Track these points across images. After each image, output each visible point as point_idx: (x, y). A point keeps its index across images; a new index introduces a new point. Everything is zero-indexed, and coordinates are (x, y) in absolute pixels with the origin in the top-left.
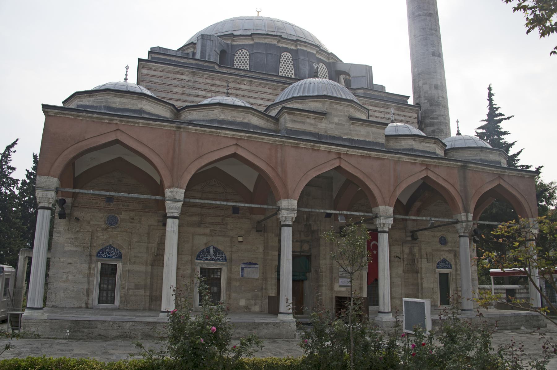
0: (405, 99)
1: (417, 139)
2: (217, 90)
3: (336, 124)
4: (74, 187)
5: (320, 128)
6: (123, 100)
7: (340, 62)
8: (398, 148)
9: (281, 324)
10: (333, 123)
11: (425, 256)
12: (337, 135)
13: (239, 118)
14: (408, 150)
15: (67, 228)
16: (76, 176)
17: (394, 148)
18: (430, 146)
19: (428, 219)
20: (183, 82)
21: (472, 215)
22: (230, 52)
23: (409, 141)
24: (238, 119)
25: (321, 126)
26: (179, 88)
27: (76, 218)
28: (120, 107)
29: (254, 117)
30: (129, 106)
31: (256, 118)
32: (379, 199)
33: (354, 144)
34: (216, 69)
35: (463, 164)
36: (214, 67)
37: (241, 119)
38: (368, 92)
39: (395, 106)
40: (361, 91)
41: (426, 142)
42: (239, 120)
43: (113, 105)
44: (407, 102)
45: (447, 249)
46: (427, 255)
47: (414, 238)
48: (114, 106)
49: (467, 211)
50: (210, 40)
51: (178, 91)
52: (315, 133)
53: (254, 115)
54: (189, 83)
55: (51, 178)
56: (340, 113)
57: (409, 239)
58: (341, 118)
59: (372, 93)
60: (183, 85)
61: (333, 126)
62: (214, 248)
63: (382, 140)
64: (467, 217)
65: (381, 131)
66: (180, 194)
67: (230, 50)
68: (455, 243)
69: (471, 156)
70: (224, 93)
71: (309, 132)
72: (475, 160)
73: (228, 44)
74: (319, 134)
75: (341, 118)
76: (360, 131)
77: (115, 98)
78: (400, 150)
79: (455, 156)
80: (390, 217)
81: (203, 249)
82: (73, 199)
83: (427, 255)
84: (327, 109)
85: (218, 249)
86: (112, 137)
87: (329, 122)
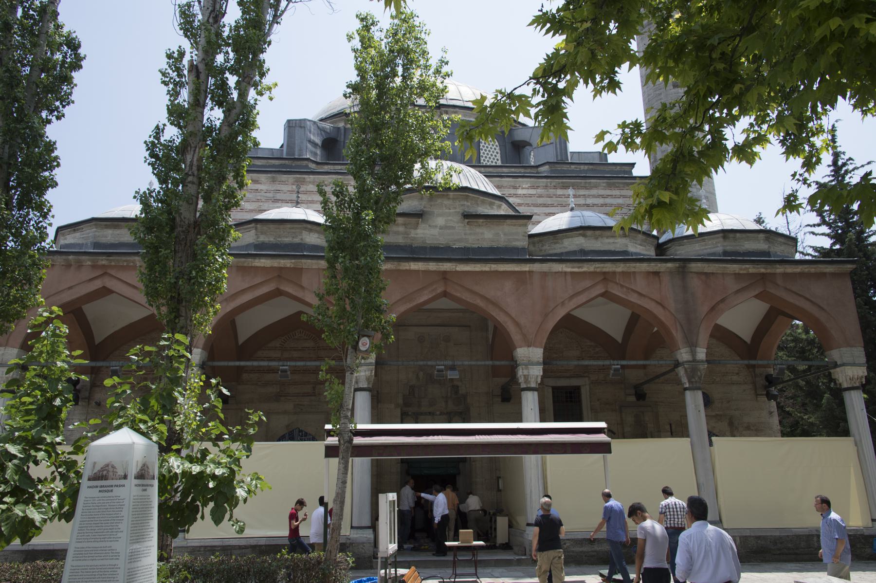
0: (627, 168)
1: (589, 233)
2: (310, 199)
3: (441, 228)
4: (239, 360)
5: (415, 238)
6: (117, 232)
7: (521, 127)
8: (558, 251)
9: (348, 545)
10: (436, 226)
11: (668, 427)
12: (442, 244)
13: (287, 237)
14: (574, 253)
15: (84, 418)
16: (240, 344)
17: (551, 252)
18: (616, 241)
19: (607, 362)
20: (258, 194)
21: (705, 350)
22: (342, 140)
23: (576, 239)
24: (286, 239)
25: (417, 234)
26: (253, 203)
27: (96, 403)
28: (113, 242)
29: (311, 234)
30: (126, 239)
31: (316, 235)
32: (516, 337)
33: (468, 255)
34: (311, 168)
35: (677, 265)
36: (307, 167)
37: (291, 239)
38: (559, 167)
39: (604, 183)
40: (546, 168)
41: (607, 237)
42: (287, 240)
43: (103, 240)
44: (632, 173)
45: (714, 414)
46: (671, 425)
47: (641, 396)
48: (104, 242)
49: (692, 346)
50: (301, 127)
51: (251, 208)
52: (406, 246)
53: (311, 230)
54: (267, 195)
55: (10, 349)
56: (447, 211)
57: (633, 399)
58: (450, 218)
59: (565, 167)
60: (259, 198)
61: (435, 232)
62: (300, 431)
63: (523, 243)
64: (693, 353)
65: (520, 230)
66: (537, 353)
67: (342, 137)
68: (729, 402)
69: (706, 249)
70: (291, 201)
71: (396, 246)
72: (714, 254)
73: (339, 128)
74: (411, 246)
75: (450, 218)
76: (482, 233)
77: (105, 230)
78: (562, 254)
79: (678, 252)
80: (538, 364)
81: (282, 434)
82: (93, 376)
83: (671, 425)
84: (425, 207)
85: (306, 433)
86: (97, 284)
87: (430, 226)
